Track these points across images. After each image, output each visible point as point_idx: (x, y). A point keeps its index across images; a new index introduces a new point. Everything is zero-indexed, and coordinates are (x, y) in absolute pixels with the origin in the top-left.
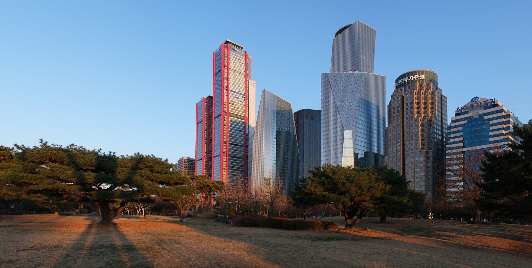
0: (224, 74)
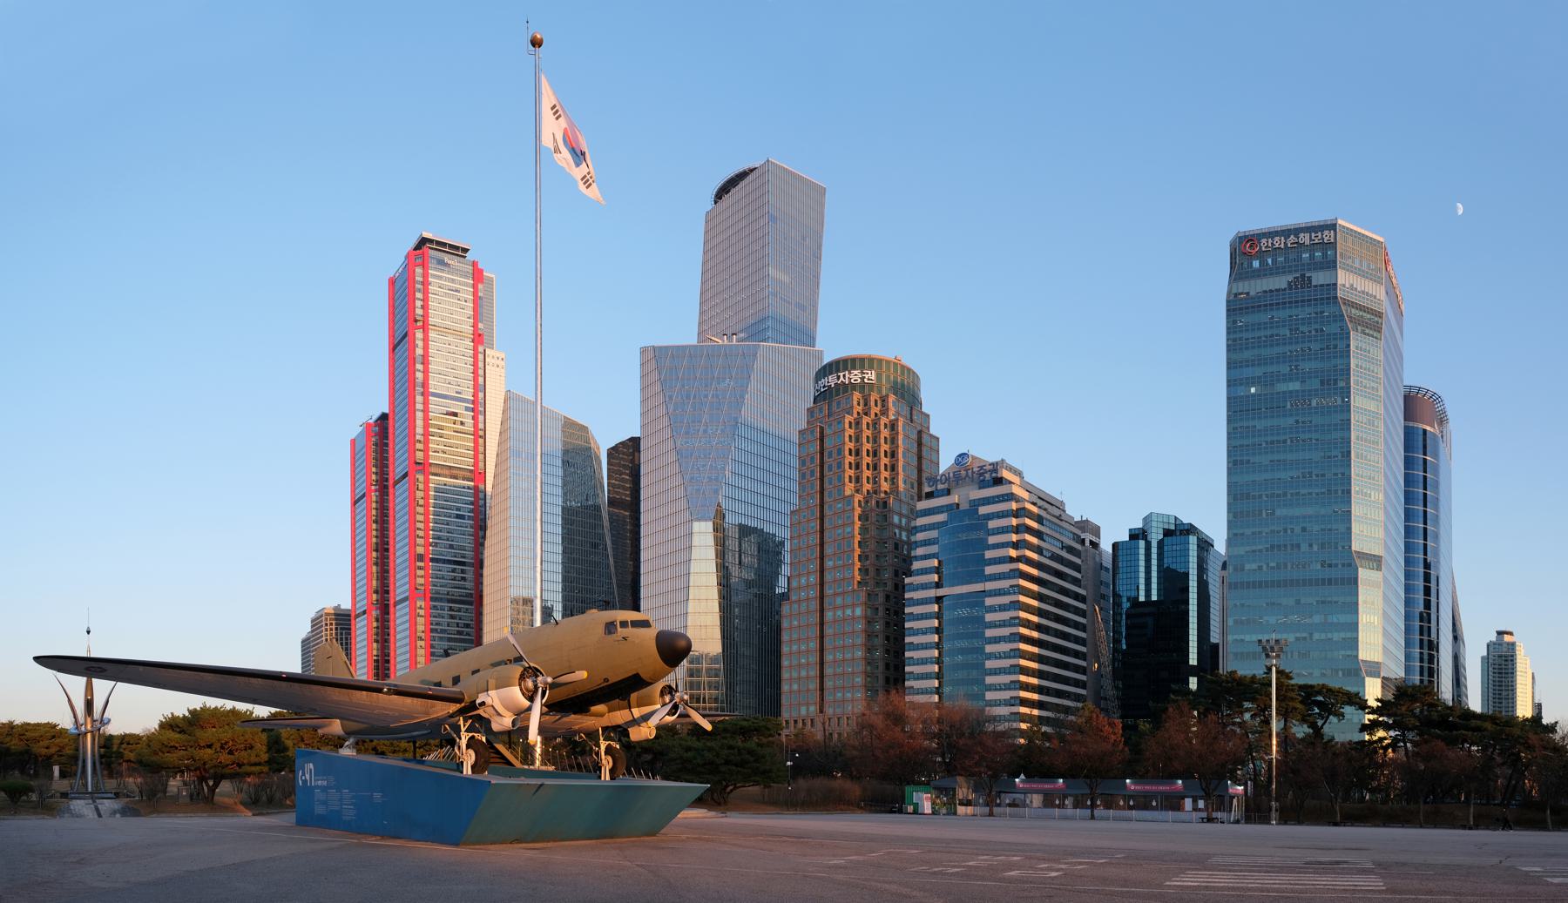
0: (415, 346)
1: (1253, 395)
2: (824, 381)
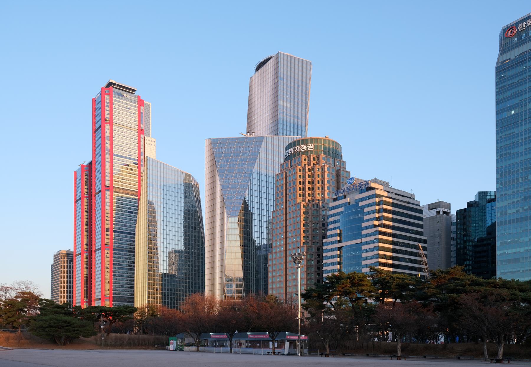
1: (514, 115)
2: (288, 151)
